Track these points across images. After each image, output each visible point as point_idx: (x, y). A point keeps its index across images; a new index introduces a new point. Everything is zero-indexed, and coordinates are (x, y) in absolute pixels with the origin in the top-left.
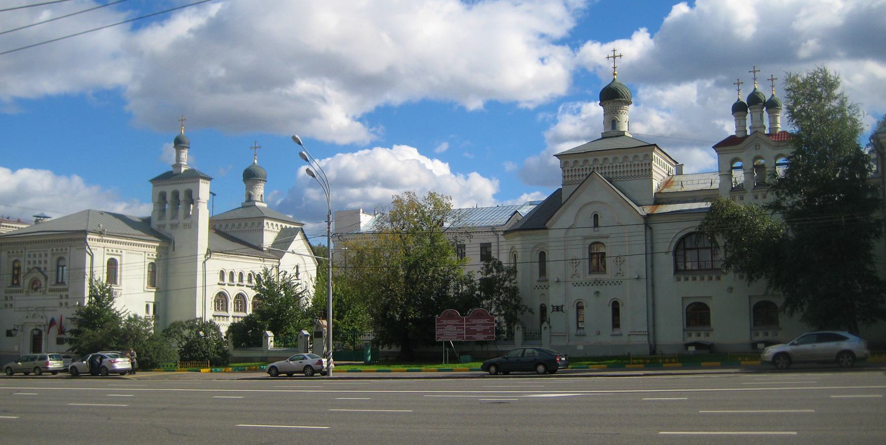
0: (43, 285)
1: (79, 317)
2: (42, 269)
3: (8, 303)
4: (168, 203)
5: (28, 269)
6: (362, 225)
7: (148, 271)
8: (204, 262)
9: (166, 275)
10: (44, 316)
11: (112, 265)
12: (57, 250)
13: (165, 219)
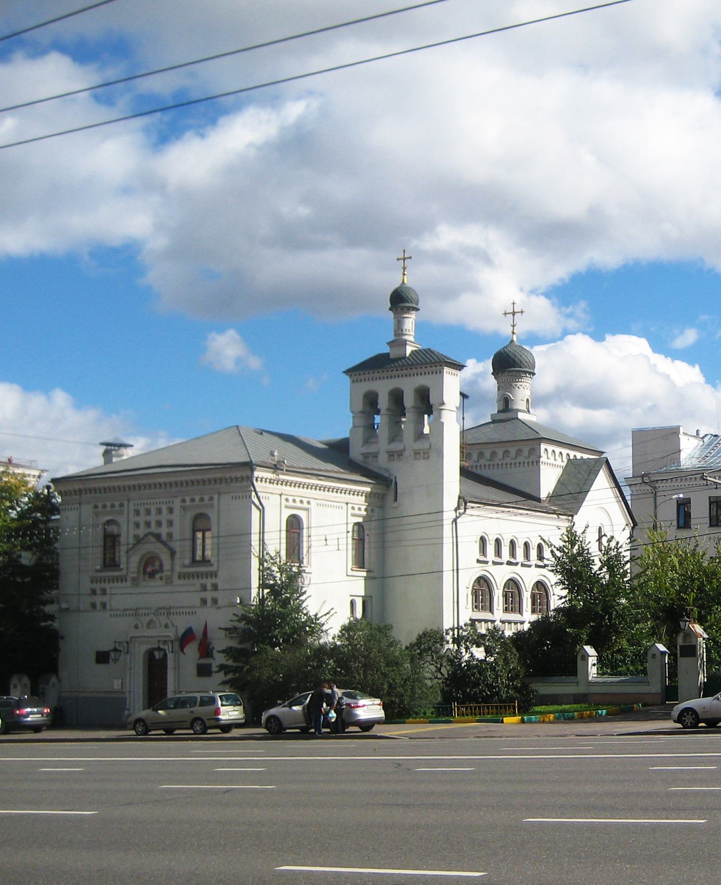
0: (167, 565)
1: (242, 625)
2: (164, 537)
3: (98, 599)
4: (382, 412)
5: (136, 537)
6: (683, 456)
7: (353, 539)
8: (455, 521)
9: (383, 546)
10: (170, 625)
11: (294, 526)
12: (193, 500)
13: (377, 443)
